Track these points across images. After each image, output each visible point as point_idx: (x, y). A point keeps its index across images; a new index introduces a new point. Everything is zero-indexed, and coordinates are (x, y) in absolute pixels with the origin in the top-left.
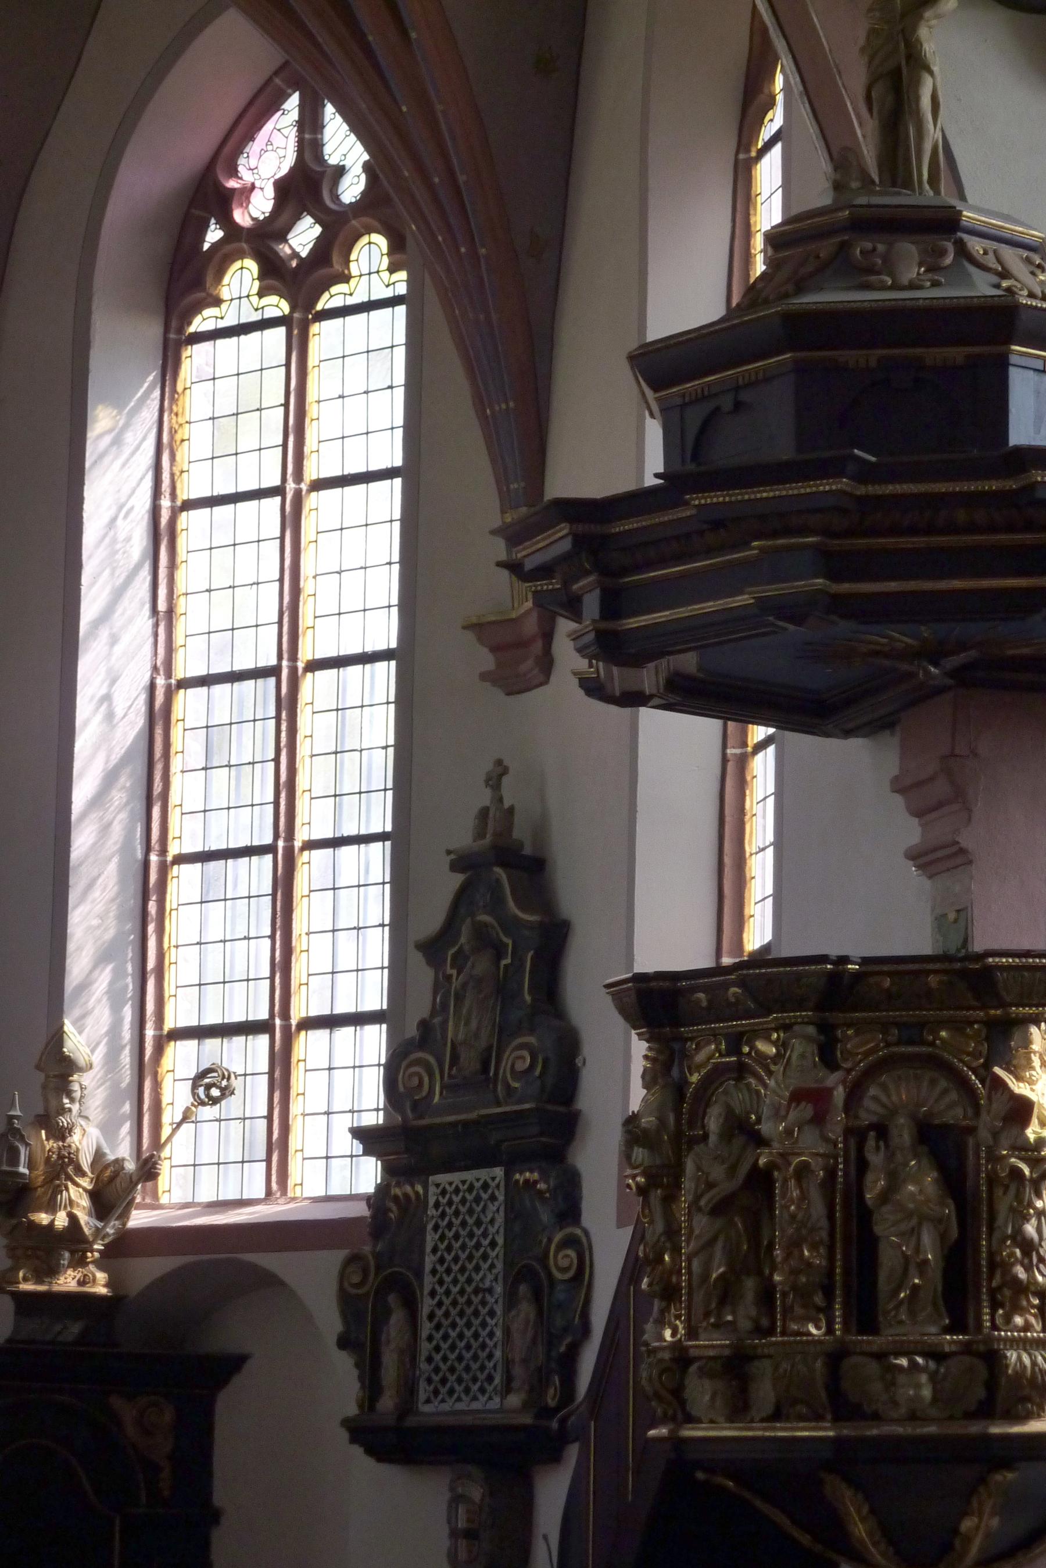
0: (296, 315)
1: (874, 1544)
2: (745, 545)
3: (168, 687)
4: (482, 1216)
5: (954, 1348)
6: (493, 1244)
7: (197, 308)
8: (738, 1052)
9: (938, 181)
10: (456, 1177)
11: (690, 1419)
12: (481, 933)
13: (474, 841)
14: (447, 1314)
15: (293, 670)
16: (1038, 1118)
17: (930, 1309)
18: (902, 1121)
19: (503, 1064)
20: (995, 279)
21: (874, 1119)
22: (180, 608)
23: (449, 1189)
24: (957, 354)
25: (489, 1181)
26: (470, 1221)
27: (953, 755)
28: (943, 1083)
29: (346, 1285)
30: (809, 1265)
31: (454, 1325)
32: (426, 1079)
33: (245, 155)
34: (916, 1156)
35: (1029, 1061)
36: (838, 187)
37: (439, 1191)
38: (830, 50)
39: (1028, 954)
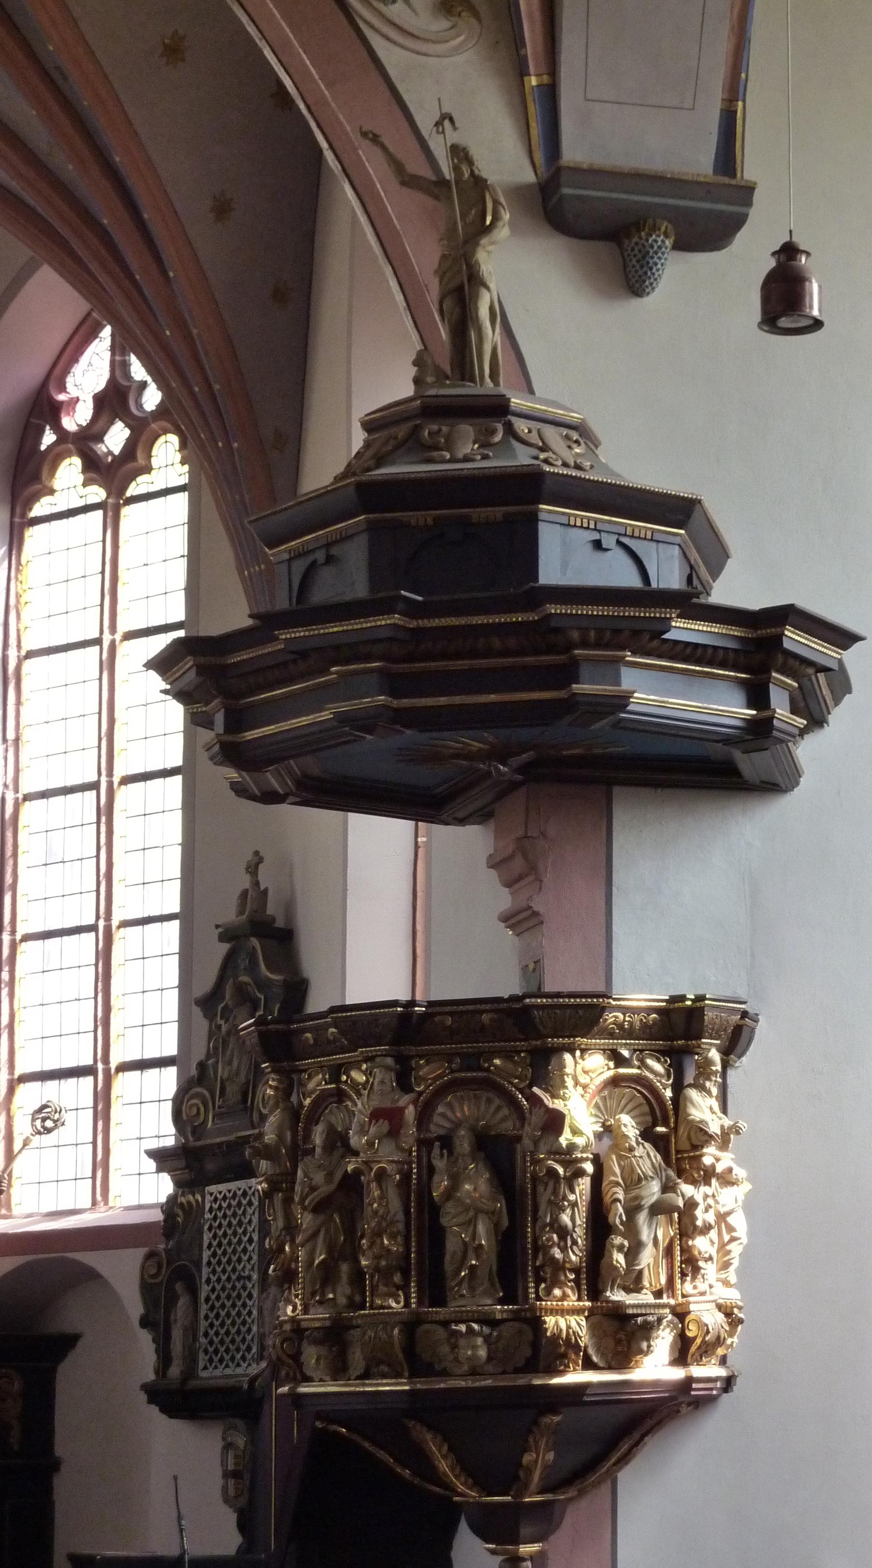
0: (110, 501)
1: (456, 1477)
2: (325, 671)
3: (17, 799)
4: (243, 1218)
5: (505, 1316)
6: (250, 1241)
7: (35, 498)
8: (337, 1080)
9: (498, 375)
10: (223, 1187)
11: (307, 1379)
12: (240, 989)
13: (237, 917)
14: (218, 1298)
15: (110, 784)
16: (570, 1127)
17: (486, 1284)
18: (463, 1133)
19: (257, 1096)
20: (535, 452)
21: (442, 1132)
22: (24, 738)
23: (220, 1197)
24: (497, 512)
25: (247, 1189)
26: (234, 1222)
27: (526, 837)
28: (497, 1102)
29: (146, 1277)
30: (389, 1251)
31: (223, 1306)
32: (202, 1109)
33: (72, 374)
34: (474, 1160)
35: (564, 1082)
36: (417, 381)
37: (212, 1198)
38: (421, 274)
39: (558, 995)
